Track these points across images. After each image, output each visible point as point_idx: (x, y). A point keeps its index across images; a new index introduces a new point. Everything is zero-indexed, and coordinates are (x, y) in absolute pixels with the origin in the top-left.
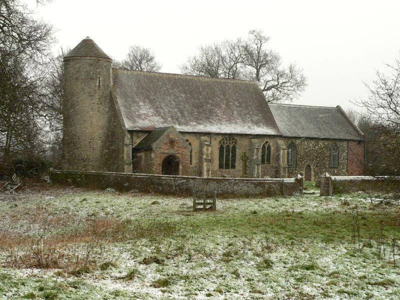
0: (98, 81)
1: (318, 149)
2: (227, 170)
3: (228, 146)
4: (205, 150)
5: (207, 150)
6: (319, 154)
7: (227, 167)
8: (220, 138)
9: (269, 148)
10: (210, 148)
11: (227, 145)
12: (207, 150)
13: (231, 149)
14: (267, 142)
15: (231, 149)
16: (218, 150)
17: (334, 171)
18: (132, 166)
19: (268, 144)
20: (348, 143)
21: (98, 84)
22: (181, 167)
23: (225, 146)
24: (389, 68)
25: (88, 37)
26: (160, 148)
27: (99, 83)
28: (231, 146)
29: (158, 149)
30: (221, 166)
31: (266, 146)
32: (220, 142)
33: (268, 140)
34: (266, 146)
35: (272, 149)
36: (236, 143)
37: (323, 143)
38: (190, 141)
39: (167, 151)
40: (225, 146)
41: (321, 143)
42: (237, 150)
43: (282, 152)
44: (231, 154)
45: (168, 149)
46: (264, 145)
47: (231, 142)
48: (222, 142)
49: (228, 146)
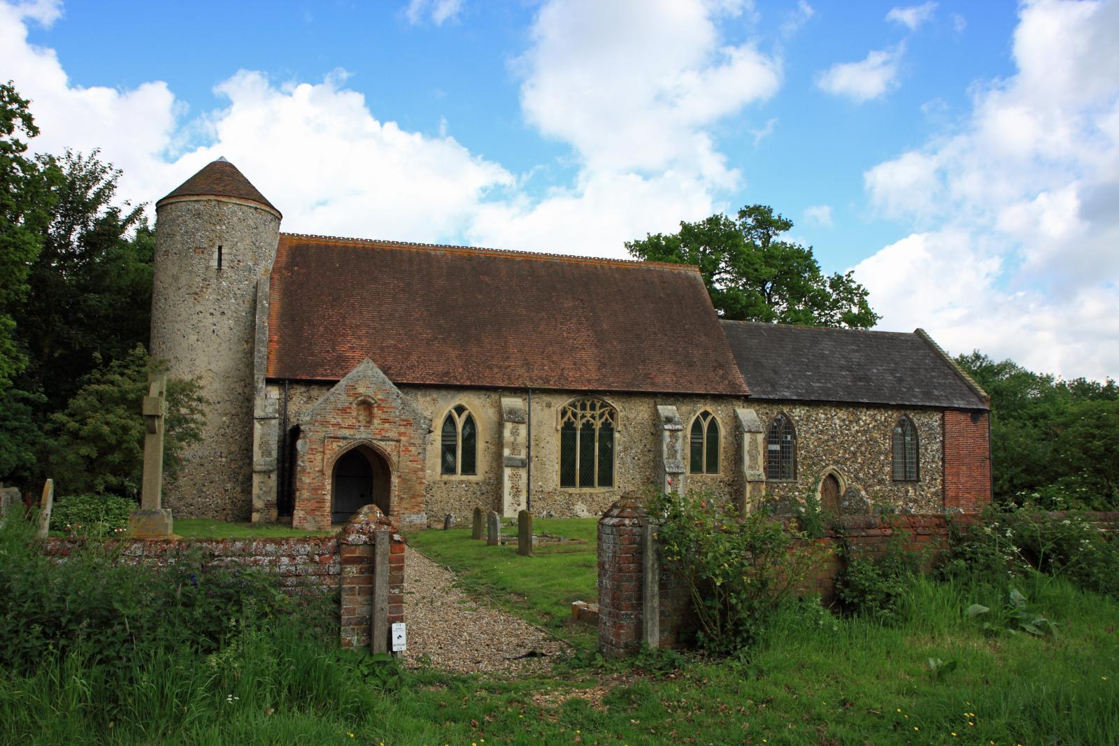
0: (216, 255)
1: (857, 432)
2: (586, 490)
3: (588, 427)
4: (507, 433)
5: (515, 433)
6: (861, 445)
7: (587, 481)
8: (561, 402)
9: (713, 427)
10: (523, 429)
11: (584, 420)
12: (515, 433)
13: (597, 434)
14: (705, 414)
15: (597, 434)
16: (559, 435)
17: (907, 491)
18: (274, 477)
19: (709, 418)
20: (943, 418)
21: (215, 264)
22: (395, 480)
23: (579, 425)
24: (810, 666)
25: (222, 157)
26: (325, 423)
27: (220, 260)
28: (598, 425)
29: (318, 427)
30: (567, 480)
31: (705, 425)
32: (564, 413)
33: (709, 409)
34: (705, 425)
35: (723, 432)
36: (612, 415)
37: (873, 418)
38: (470, 409)
39: (347, 433)
40: (579, 425)
41: (865, 416)
42: (617, 435)
43: (747, 437)
44: (597, 445)
45: (351, 427)
46: (450, 420)
47: (598, 412)
48: (569, 414)
49: (588, 427)
